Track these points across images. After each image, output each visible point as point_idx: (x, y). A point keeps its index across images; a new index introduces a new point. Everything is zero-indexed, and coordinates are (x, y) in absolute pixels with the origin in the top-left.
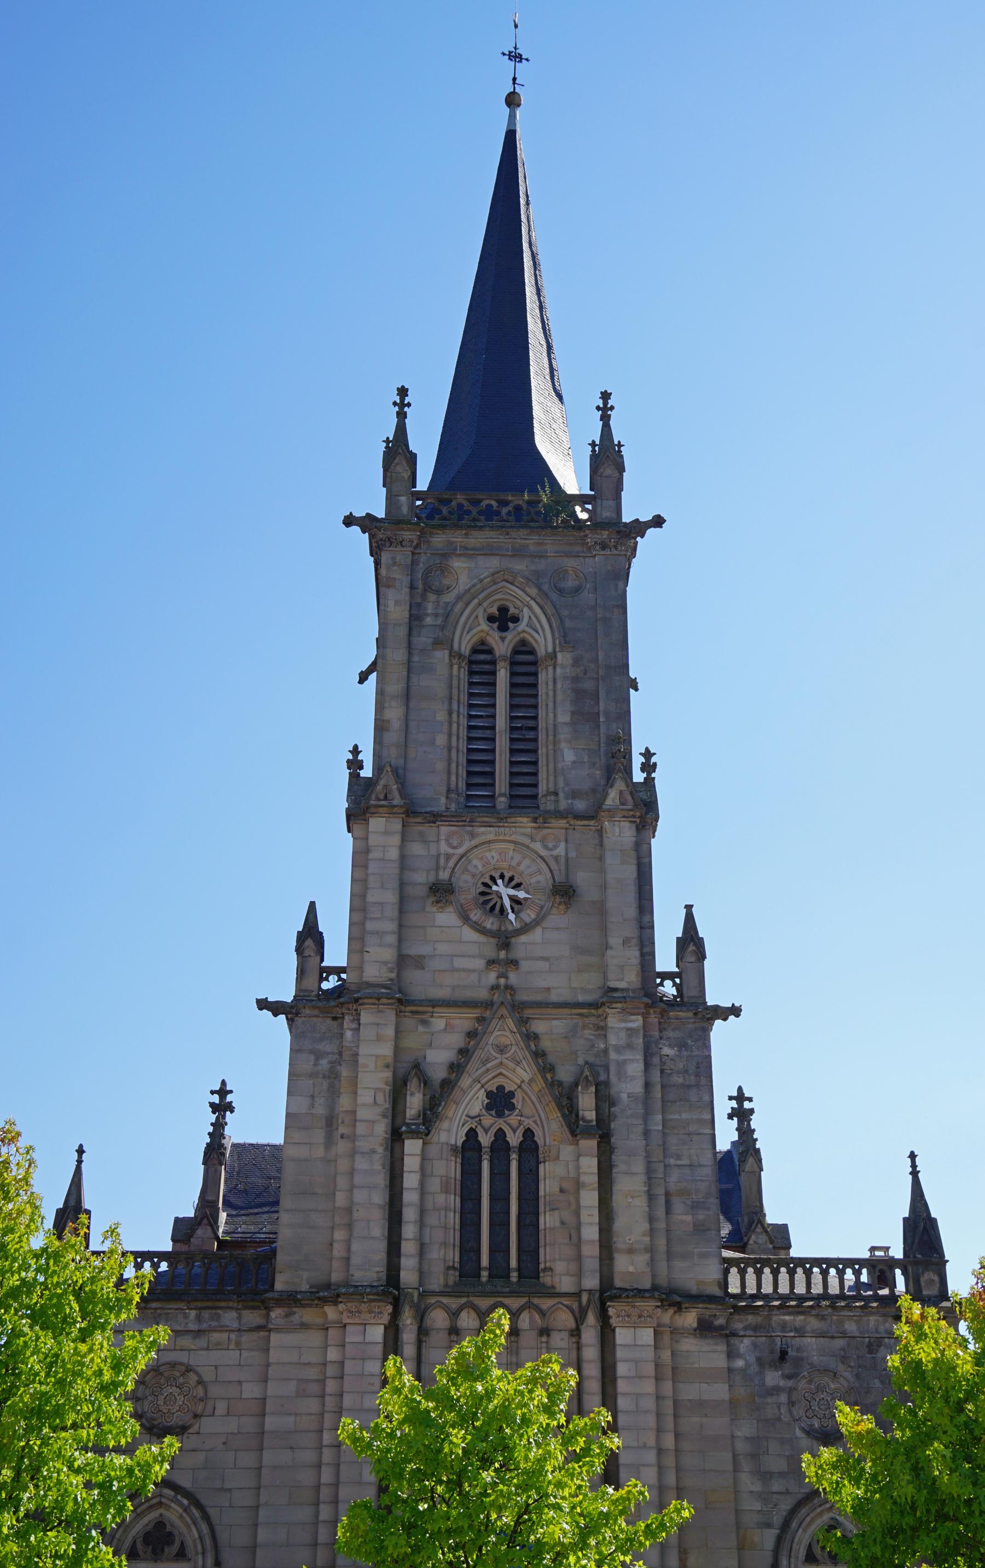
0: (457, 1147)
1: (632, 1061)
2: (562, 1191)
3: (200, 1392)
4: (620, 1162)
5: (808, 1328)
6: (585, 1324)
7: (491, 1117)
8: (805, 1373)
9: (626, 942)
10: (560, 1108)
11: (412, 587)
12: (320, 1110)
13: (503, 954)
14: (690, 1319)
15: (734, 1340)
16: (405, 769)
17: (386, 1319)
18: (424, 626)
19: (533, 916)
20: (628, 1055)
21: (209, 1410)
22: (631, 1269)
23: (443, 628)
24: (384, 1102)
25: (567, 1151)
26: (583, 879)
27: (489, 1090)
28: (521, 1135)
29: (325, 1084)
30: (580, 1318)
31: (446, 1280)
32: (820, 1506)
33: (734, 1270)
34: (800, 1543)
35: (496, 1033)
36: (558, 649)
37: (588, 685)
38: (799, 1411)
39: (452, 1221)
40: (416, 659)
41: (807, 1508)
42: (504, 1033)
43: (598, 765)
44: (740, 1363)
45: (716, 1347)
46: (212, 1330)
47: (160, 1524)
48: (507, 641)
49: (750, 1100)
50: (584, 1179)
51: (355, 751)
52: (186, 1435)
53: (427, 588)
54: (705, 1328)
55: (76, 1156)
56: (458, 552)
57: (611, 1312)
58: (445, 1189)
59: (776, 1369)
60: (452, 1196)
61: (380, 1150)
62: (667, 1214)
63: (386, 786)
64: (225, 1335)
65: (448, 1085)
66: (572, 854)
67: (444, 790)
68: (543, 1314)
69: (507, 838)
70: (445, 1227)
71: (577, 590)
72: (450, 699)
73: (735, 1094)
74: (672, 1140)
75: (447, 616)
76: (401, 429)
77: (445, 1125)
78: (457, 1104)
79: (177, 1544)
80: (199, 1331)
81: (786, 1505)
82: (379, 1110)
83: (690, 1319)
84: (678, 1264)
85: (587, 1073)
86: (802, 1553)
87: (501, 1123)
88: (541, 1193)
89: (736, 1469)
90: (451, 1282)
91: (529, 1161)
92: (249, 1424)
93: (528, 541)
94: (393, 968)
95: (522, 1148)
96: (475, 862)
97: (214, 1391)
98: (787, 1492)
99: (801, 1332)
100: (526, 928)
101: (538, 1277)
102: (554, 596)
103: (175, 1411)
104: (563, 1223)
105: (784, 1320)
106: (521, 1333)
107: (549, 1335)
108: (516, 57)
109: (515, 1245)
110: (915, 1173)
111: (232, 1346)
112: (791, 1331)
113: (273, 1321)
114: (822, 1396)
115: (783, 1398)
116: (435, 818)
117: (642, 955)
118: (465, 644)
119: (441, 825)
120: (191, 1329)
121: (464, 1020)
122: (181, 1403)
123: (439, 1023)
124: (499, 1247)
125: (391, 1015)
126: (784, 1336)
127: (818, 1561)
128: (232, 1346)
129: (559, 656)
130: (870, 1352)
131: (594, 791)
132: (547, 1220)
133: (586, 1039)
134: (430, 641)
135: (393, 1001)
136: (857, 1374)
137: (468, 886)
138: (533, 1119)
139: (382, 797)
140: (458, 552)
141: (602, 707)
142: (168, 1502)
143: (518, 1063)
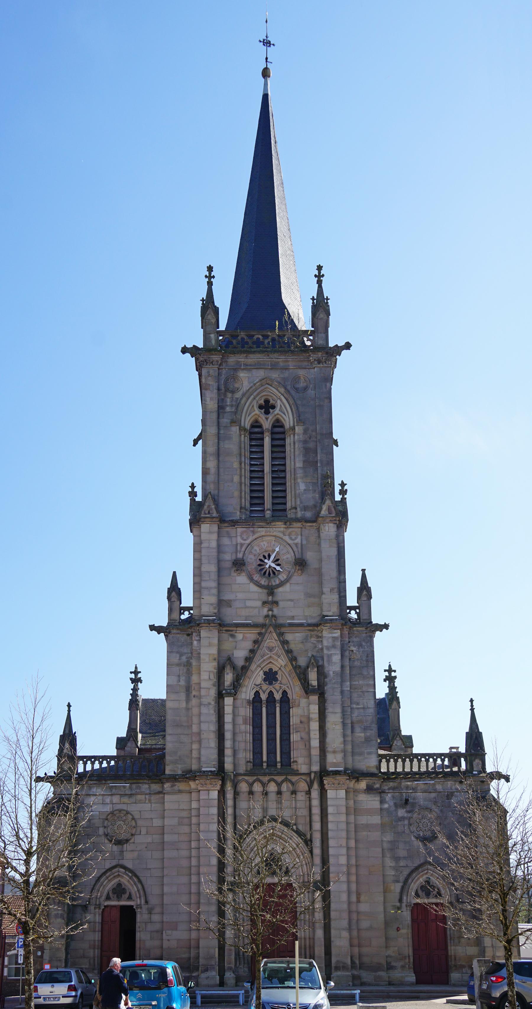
1: (335, 654)
2: (301, 722)
8: (417, 810)
9: (332, 590)
12: (182, 683)
13: (270, 598)
15: (383, 795)
16: (218, 496)
17: (218, 787)
18: (225, 412)
19: (285, 577)
20: (333, 651)
21: (138, 832)
22: (335, 761)
23: (235, 413)
24: (214, 679)
25: (303, 702)
26: (310, 556)
27: (265, 671)
28: (281, 694)
30: (310, 786)
31: (246, 767)
33: (384, 760)
34: (412, 889)
35: (268, 641)
36: (296, 424)
37: (311, 445)
38: (413, 828)
39: (249, 738)
41: (416, 873)
42: (272, 640)
43: (317, 491)
44: (386, 806)
47: (119, 885)
48: (269, 420)
51: (193, 486)
52: (128, 844)
54: (370, 789)
56: (242, 367)
60: (248, 726)
61: (213, 703)
62: (352, 732)
64: (143, 796)
65: (245, 669)
68: (293, 784)
70: (245, 742)
72: (240, 455)
73: (387, 668)
74: (355, 695)
77: (244, 689)
81: (406, 872)
82: (211, 683)
83: (363, 785)
84: (357, 758)
85: (313, 661)
87: (271, 688)
88: (291, 723)
89: (383, 856)
90: (249, 769)
92: (157, 838)
93: (279, 360)
97: (140, 823)
98: (407, 866)
99: (415, 790)
100: (282, 584)
101: (290, 766)
102: (293, 392)
104: (302, 738)
107: (296, 794)
111: (147, 802)
112: (411, 790)
115: (406, 822)
116: (234, 523)
121: (252, 634)
124: (271, 752)
128: (147, 802)
129: (297, 428)
130: (448, 799)
131: (315, 506)
132: (295, 737)
134: (229, 421)
137: (252, 560)
138: (287, 685)
139: (207, 512)
140: (242, 367)
141: (319, 458)
142: (122, 875)
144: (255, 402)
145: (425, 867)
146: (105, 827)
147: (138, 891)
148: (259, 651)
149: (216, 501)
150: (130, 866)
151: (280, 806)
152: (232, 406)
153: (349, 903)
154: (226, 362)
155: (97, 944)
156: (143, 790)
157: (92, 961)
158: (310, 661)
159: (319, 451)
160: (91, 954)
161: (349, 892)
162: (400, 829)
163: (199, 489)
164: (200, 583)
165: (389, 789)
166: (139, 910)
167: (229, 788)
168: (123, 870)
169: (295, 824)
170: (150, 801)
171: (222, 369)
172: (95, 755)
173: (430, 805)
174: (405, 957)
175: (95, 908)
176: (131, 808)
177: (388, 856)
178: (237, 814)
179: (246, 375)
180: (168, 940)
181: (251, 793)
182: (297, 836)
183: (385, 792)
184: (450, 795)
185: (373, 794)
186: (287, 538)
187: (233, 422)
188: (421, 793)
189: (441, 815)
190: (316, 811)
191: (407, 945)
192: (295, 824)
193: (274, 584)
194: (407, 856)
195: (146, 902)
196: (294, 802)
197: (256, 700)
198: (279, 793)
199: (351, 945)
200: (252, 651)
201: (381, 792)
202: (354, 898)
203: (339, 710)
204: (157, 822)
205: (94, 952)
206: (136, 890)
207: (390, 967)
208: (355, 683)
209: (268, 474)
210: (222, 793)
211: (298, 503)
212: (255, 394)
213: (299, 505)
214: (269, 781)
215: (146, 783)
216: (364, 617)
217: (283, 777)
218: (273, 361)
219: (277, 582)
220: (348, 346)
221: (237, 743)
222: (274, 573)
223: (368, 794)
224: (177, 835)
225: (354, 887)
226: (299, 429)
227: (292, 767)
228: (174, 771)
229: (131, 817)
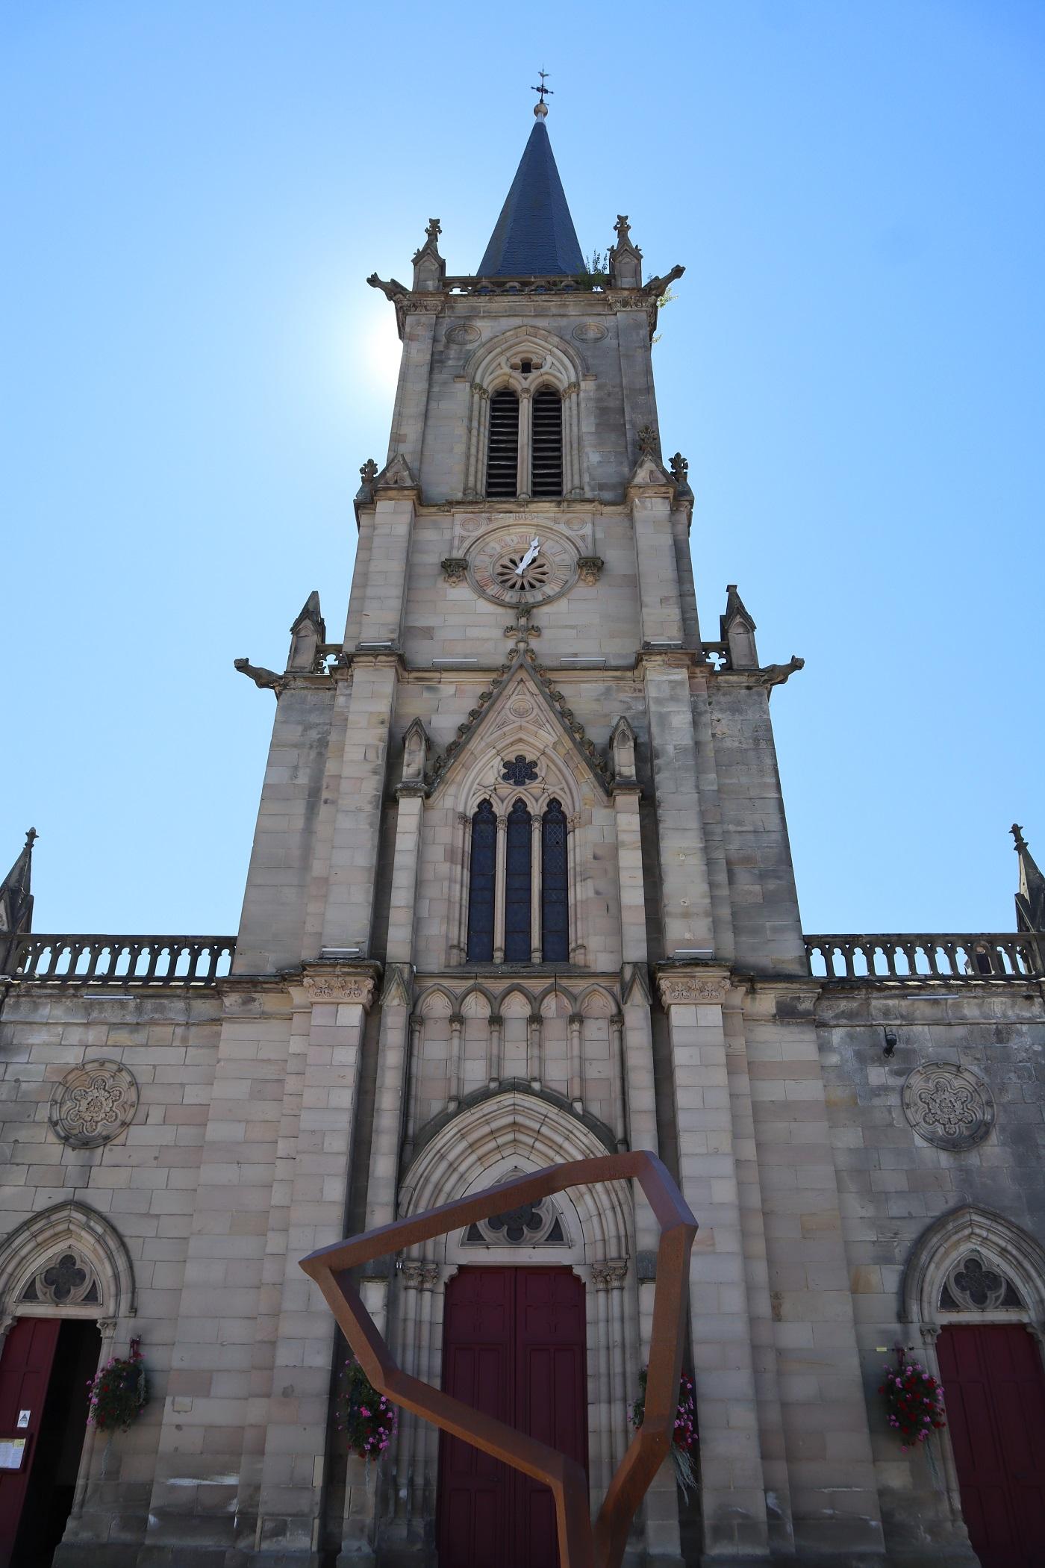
2: (595, 857)
5: (918, 1014)
6: (629, 1004)
7: (508, 786)
10: (592, 766)
11: (435, 340)
12: (303, 779)
13: (523, 621)
16: (420, 470)
17: (364, 997)
18: (445, 367)
19: (557, 589)
20: (671, 707)
25: (600, 815)
26: (613, 557)
27: (506, 759)
28: (545, 805)
29: (313, 754)
30: (621, 999)
31: (448, 959)
32: (956, 1233)
33: (816, 952)
34: (932, 1284)
35: (514, 697)
36: (581, 378)
37: (612, 403)
38: (915, 1116)
39: (458, 894)
40: (436, 389)
41: (939, 1236)
42: (524, 697)
44: (834, 1059)
45: (802, 1036)
46: (153, 1023)
47: (68, 1260)
48: (529, 380)
50: (622, 837)
52: (108, 1147)
53: (450, 340)
54: (786, 1014)
55: (26, 839)
56: (482, 314)
57: (664, 984)
58: (451, 856)
59: (882, 1065)
60: (459, 867)
61: (368, 808)
64: (170, 1029)
65: (455, 749)
66: (599, 535)
68: (573, 998)
69: (528, 522)
70: (449, 901)
75: (467, 361)
77: (452, 790)
78: (468, 769)
79: (87, 1286)
80: (138, 1024)
81: (909, 1234)
82: (369, 767)
83: (767, 1002)
87: (520, 792)
88: (570, 865)
89: (840, 1189)
90: (454, 962)
91: (555, 833)
93: (550, 303)
94: (395, 630)
95: (545, 819)
96: (492, 544)
97: (147, 1094)
98: (910, 1217)
99: (909, 1020)
100: (548, 600)
101: (567, 958)
103: (100, 1118)
104: (597, 893)
105: (887, 1006)
106: (545, 1022)
107: (581, 1022)
108: (542, 90)
109: (537, 919)
110: (1021, 847)
111: (177, 1043)
112: (896, 1018)
113: (227, 1009)
114: (943, 1097)
115: (893, 1100)
117: (683, 612)
119: (457, 512)
120: (129, 1022)
121: (476, 685)
122: (108, 1110)
123: (447, 689)
125: (390, 674)
126: (887, 1025)
127: (958, 1306)
128: (177, 1043)
129: (583, 384)
130: (1000, 1041)
132: (579, 893)
133: (621, 701)
135: (393, 659)
136: (985, 1068)
137: (483, 563)
138: (561, 786)
140: (482, 314)
142: (78, 1230)
143: (541, 726)
148: (492, 715)
150: (102, 1206)
153: (753, 1321)
154: (452, 307)
156: (172, 1015)
159: (627, 409)
161: (750, 1290)
167: (396, 1002)
168: (80, 1217)
170: (185, 1040)
171: (444, 317)
173: (953, 1056)
180: (179, 1427)
181: (457, 1018)
182: (585, 1130)
184: (1002, 1033)
185: (797, 1024)
186: (562, 528)
188: (926, 1028)
189: (986, 1080)
190: (641, 1059)
192: (581, 1099)
195: (134, 1309)
196: (576, 1041)
197: (483, 819)
199: (765, 1456)
200: (474, 714)
202: (764, 1307)
203: (693, 823)
204: (193, 1095)
208: (728, 781)
209: (526, 447)
210: (373, 1012)
213: (588, 483)
214: (508, 992)
216: (739, 659)
218: (539, 305)
219: (540, 598)
221: (425, 904)
223: (782, 1024)
224: (243, 1124)
225: (761, 1271)
227: (571, 961)
229: (129, 1079)
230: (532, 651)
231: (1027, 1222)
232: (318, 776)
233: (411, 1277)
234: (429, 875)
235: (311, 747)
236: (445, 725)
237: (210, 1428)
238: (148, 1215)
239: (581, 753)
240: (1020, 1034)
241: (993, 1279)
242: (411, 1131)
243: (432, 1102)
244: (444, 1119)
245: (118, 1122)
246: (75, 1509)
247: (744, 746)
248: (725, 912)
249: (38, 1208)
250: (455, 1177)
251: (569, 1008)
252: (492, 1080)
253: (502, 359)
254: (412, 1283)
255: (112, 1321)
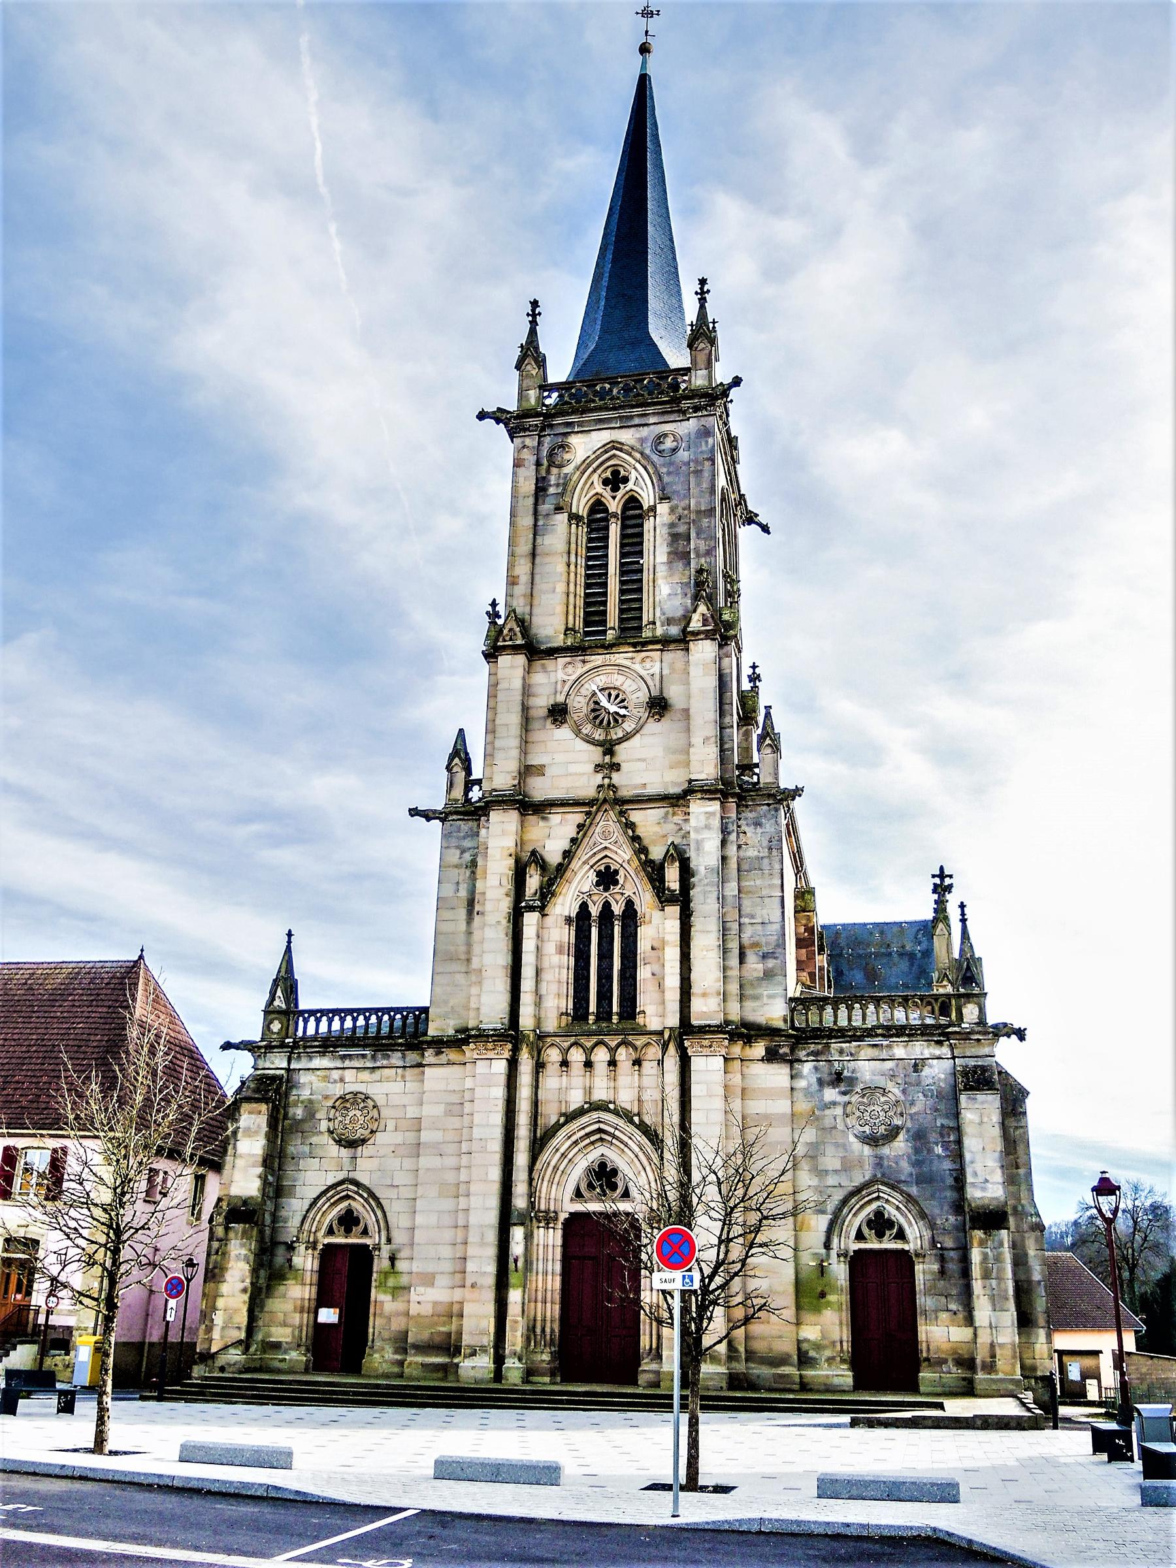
0: (570, 917)
1: (709, 839)
2: (653, 948)
3: (375, 1113)
4: (697, 922)
8: (859, 1090)
9: (706, 740)
11: (538, 464)
12: (463, 893)
13: (607, 759)
14: (759, 1049)
15: (796, 1065)
17: (507, 1055)
19: (634, 726)
20: (706, 834)
21: (382, 1127)
22: (705, 1009)
23: (562, 494)
24: (508, 886)
25: (657, 915)
26: (673, 693)
29: (468, 873)
35: (601, 823)
37: (682, 529)
40: (540, 523)
43: (689, 595)
45: (780, 1071)
47: (349, 1212)
48: (617, 499)
49: (951, 876)
50: (667, 938)
51: (494, 604)
53: (551, 464)
54: (772, 1056)
60: (566, 956)
61: (504, 922)
62: (741, 963)
63: (511, 630)
65: (561, 869)
67: (563, 628)
68: (635, 1048)
70: (560, 982)
71: (674, 450)
72: (569, 553)
73: (938, 873)
74: (747, 903)
75: (565, 485)
76: (533, 332)
79: (362, 1225)
81: (838, 1196)
82: (504, 891)
83: (759, 1049)
84: (748, 1004)
85: (672, 851)
86: (853, 1234)
88: (639, 952)
90: (563, 1025)
92: (410, 1137)
97: (385, 1113)
99: (854, 1057)
100: (627, 737)
101: (634, 1019)
102: (655, 458)
106: (618, 1063)
115: (839, 1111)
116: (552, 652)
118: (581, 506)
121: (576, 817)
124: (604, 995)
129: (658, 506)
130: (916, 1071)
131: (684, 616)
132: (643, 973)
134: (552, 507)
137: (579, 705)
139: (508, 638)
141: (692, 547)
144: (596, 476)
145: (873, 1188)
146: (330, 1120)
147: (377, 1221)
149: (521, 622)
151: (612, 1084)
152: (558, 485)
155: (307, 1304)
157: (297, 1333)
158: (668, 851)
159: (693, 535)
160: (297, 1322)
162: (828, 1122)
163: (501, 609)
164: (493, 743)
165: (808, 1055)
166: (377, 1253)
169: (638, 1114)
172: (323, 1007)
173: (881, 1082)
174: (834, 1343)
175: (307, 1248)
176: (371, 1090)
177: (806, 1168)
178: (539, 1097)
179: (582, 440)
181: (565, 1063)
182: (640, 1134)
183: (801, 1061)
187: (559, 509)
189: (903, 1098)
191: (838, 1323)
192: (638, 1114)
193: (615, 737)
194: (839, 1168)
195: (389, 1241)
198: (613, 1063)
201: (792, 1062)
204: (412, 1112)
205: (302, 1318)
206: (374, 1219)
207: (804, 1360)
210: (513, 1064)
211: (658, 614)
212: (594, 465)
214: (596, 1045)
215: (397, 1050)
217: (619, 1038)
219: (620, 735)
220: (737, 382)
222: (616, 721)
226: (663, 509)
228: (443, 1030)
230: (614, 786)
231: (914, 1190)
232: (472, 891)
233: (540, 1221)
234: (546, 964)
235: (467, 867)
236: (553, 853)
237: (435, 1303)
238: (392, 1186)
239: (645, 870)
240: (931, 1066)
241: (890, 1224)
242: (538, 1135)
243: (551, 1115)
244: (558, 1127)
245: (369, 1130)
246: (370, 1343)
247: (761, 855)
248: (734, 988)
249: (329, 1183)
250: (566, 1161)
251: (634, 1056)
252: (586, 1103)
253: (595, 477)
254: (541, 1225)
255: (378, 1247)
